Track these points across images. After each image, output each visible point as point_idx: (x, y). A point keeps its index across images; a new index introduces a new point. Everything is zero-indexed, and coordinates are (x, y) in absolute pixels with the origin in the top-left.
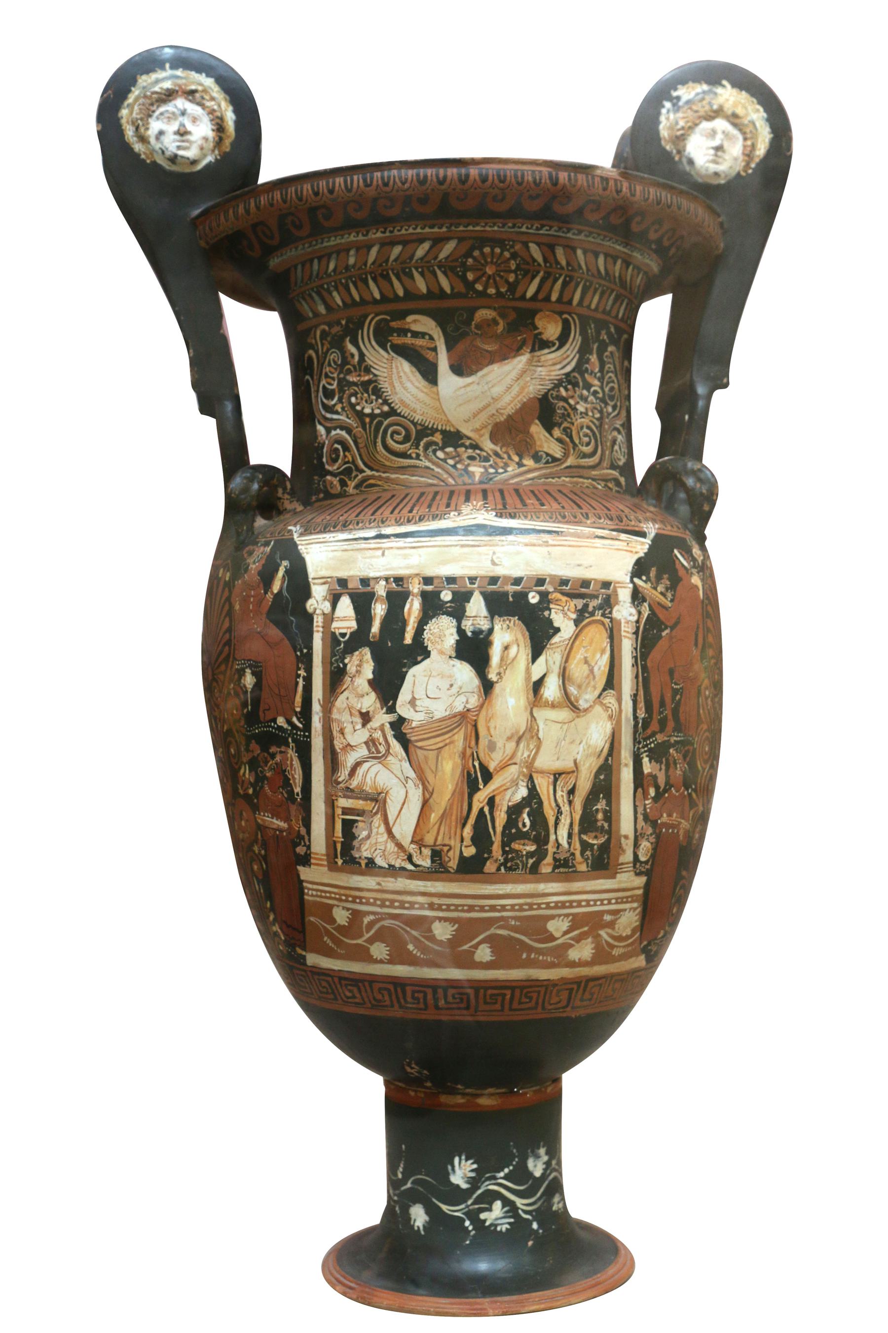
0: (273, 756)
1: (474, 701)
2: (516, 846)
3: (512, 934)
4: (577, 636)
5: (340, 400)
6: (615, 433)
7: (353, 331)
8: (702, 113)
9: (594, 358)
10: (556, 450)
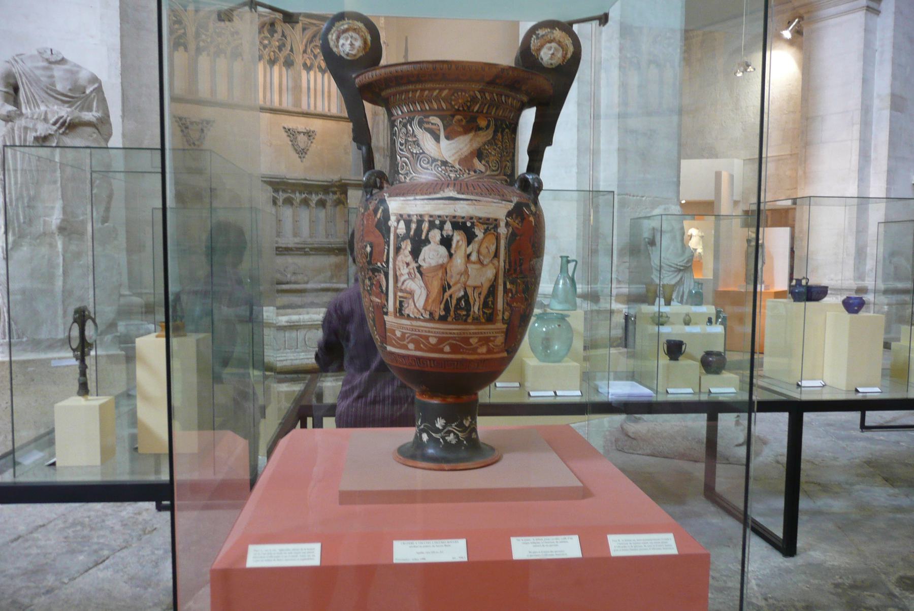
0: (376, 276)
1: (446, 260)
2: (459, 312)
3: (458, 343)
4: (484, 238)
5: (405, 147)
6: (507, 163)
7: (410, 121)
8: (547, 40)
9: (499, 134)
10: (483, 169)
